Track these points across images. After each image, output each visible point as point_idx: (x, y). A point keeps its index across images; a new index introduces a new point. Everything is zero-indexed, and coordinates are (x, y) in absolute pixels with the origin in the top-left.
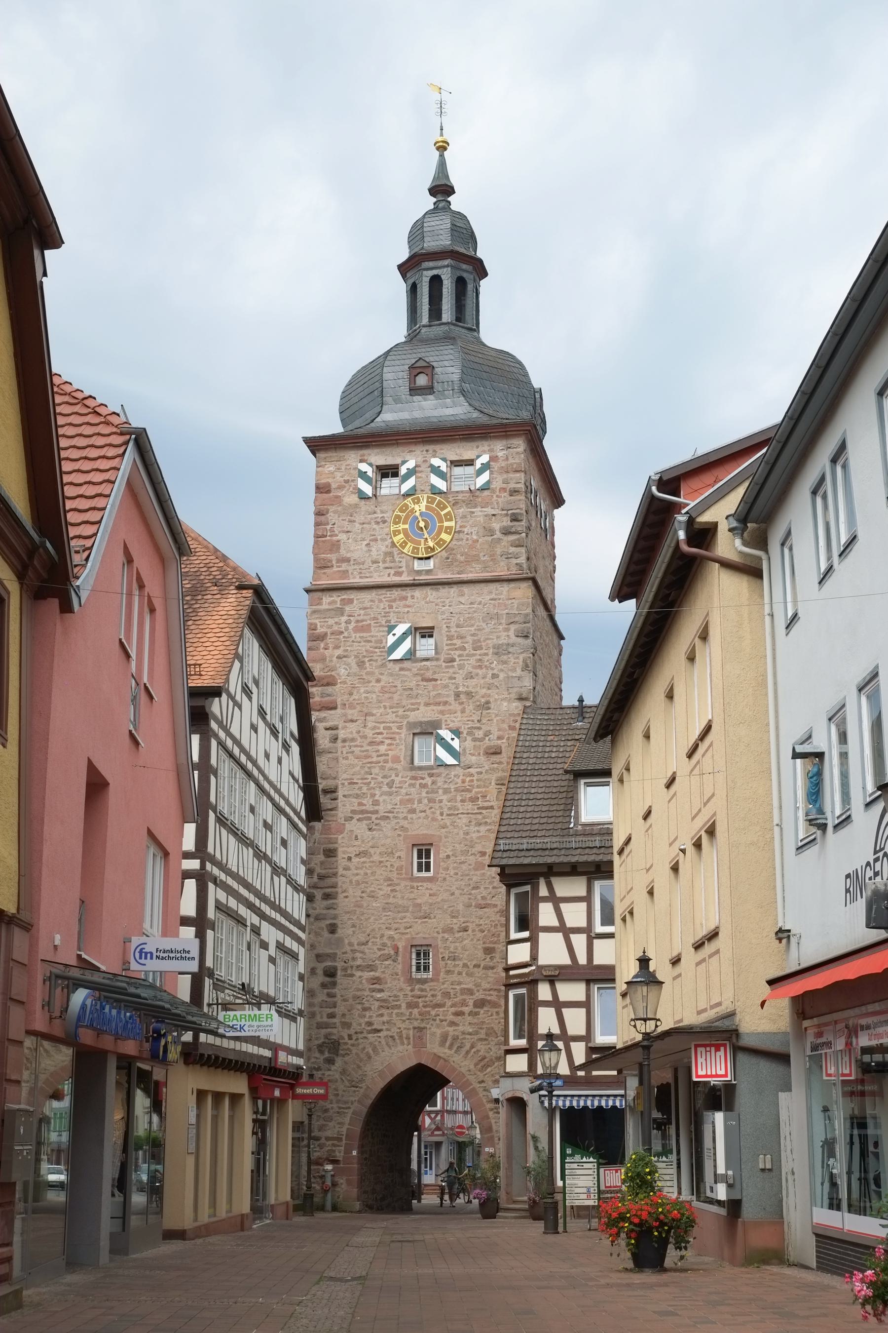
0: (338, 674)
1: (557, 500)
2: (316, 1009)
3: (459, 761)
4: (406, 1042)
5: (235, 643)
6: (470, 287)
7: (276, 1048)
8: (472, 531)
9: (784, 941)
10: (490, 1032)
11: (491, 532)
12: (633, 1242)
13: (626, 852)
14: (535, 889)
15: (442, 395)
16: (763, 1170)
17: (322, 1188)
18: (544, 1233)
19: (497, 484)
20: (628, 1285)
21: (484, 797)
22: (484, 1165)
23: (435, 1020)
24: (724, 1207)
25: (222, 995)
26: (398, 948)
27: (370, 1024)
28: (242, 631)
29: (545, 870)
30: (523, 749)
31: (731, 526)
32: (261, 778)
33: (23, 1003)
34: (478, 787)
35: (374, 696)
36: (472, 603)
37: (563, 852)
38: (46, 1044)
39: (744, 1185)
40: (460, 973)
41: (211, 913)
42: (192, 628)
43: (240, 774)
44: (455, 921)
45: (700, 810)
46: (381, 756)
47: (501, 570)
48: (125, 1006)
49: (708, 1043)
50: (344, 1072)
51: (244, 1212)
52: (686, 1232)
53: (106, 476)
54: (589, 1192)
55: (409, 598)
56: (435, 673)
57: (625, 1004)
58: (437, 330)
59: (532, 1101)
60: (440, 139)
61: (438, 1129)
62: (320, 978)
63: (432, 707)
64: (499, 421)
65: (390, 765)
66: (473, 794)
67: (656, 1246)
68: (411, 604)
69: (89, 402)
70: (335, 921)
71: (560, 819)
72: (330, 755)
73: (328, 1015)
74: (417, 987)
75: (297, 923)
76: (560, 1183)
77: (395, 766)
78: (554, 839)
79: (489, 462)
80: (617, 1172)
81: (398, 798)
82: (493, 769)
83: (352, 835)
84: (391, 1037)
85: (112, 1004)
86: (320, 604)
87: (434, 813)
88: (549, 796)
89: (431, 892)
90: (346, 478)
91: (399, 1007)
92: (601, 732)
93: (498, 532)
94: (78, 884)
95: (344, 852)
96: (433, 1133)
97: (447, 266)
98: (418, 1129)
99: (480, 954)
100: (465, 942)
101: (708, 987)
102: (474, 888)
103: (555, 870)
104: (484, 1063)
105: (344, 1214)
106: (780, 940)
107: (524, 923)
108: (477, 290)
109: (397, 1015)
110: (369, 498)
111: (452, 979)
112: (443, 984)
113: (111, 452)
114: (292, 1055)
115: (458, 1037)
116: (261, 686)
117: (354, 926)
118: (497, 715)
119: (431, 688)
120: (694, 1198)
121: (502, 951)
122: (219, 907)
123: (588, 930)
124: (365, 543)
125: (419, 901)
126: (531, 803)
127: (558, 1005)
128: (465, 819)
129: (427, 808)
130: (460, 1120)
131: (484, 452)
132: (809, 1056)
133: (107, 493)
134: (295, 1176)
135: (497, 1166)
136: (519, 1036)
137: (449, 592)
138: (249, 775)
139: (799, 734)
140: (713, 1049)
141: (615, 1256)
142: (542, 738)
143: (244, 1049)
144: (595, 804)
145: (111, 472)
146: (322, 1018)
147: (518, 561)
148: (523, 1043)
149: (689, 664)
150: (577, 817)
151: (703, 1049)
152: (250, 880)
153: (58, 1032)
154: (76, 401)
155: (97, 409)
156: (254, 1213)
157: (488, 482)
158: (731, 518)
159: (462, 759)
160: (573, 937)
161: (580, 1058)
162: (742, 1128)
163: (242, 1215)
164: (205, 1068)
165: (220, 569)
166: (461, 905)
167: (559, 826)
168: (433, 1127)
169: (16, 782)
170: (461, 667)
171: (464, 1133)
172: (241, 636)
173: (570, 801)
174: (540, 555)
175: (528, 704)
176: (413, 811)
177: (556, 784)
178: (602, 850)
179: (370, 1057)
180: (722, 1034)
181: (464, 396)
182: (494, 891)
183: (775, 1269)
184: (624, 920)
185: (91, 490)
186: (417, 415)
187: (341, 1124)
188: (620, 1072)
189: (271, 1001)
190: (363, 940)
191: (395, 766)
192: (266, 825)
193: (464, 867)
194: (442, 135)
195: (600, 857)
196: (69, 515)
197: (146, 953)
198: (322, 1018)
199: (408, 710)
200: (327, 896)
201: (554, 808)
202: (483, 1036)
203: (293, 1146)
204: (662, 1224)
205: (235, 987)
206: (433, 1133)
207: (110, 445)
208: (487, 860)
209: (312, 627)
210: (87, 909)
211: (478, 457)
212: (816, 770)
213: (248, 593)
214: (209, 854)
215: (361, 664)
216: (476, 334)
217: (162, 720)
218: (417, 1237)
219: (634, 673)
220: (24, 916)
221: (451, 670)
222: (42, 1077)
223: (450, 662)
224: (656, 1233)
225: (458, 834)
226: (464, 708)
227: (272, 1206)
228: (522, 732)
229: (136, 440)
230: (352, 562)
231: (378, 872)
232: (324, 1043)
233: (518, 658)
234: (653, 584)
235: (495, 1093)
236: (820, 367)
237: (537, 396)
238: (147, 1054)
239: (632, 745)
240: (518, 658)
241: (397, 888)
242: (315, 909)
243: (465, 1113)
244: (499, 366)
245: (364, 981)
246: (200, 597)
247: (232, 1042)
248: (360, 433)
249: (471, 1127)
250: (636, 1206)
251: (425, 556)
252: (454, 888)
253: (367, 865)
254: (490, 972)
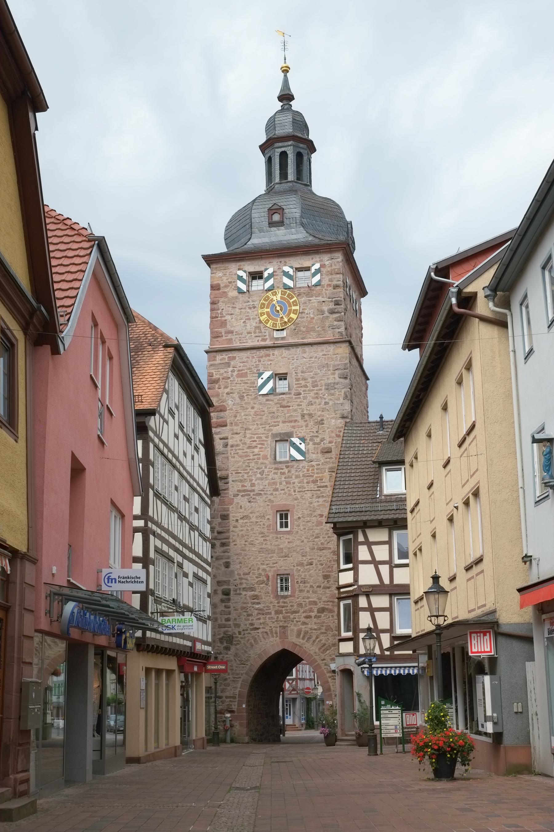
0: (227, 404)
1: (363, 292)
2: (218, 616)
3: (305, 458)
4: (275, 635)
5: (164, 381)
6: (305, 158)
7: (194, 640)
8: (310, 312)
9: (528, 563)
10: (328, 628)
11: (322, 312)
12: (434, 761)
13: (416, 511)
14: (356, 537)
15: (289, 227)
16: (516, 713)
17: (224, 729)
18: (368, 755)
19: (325, 282)
20: (434, 790)
21: (321, 480)
22: (327, 713)
23: (293, 621)
24: (490, 737)
25: (160, 607)
26: (269, 576)
27: (252, 624)
28: (168, 374)
29: (362, 525)
30: (345, 449)
31: (486, 294)
32: (181, 469)
33: (33, 611)
35: (250, 418)
36: (311, 358)
37: (373, 513)
38: (49, 639)
39: (505, 723)
40: (308, 592)
41: (152, 554)
42: (135, 372)
43: (168, 467)
44: (304, 558)
45: (468, 480)
46: (255, 455)
47: (329, 337)
48: (99, 613)
49: (479, 630)
50: (236, 655)
51: (176, 745)
52: (468, 754)
53: (79, 268)
54: (396, 728)
55: (271, 355)
56: (288, 402)
57: (417, 608)
58: (285, 186)
59: (357, 670)
60: (284, 65)
61: (294, 690)
62: (220, 596)
63: (287, 424)
64: (326, 242)
65: (261, 461)
66: (314, 478)
67: (449, 763)
68: (272, 359)
69: (68, 222)
70: (228, 560)
71: (371, 492)
72: (223, 456)
73: (225, 619)
74: (281, 600)
75: (205, 561)
76: (376, 723)
77: (265, 461)
78: (367, 505)
79: (320, 268)
80: (413, 715)
81: (267, 482)
82: (326, 462)
83: (238, 506)
84: (266, 632)
85: (91, 612)
86: (215, 360)
87: (289, 491)
88: (363, 478)
89: (289, 540)
90: (230, 280)
91: (270, 613)
92: (398, 434)
93: (326, 313)
94: (67, 533)
95: (233, 517)
96: (291, 692)
97: (291, 145)
98: (283, 690)
99: (321, 579)
100: (311, 572)
101: (476, 595)
102: (316, 538)
103: (368, 525)
104: (324, 648)
105: (238, 744)
106: (525, 562)
107: (349, 559)
108: (309, 160)
109: (269, 618)
110: (244, 292)
111: (303, 595)
112: (298, 598)
113: (82, 253)
114: (204, 645)
115: (308, 632)
116: (180, 409)
117: (240, 563)
118: (328, 428)
119: (286, 412)
120: (468, 731)
121: (335, 577)
122: (157, 550)
123: (390, 562)
124: (243, 321)
125: (281, 546)
126: (351, 483)
127: (372, 610)
128: (309, 494)
129: (285, 488)
130: (307, 684)
131: (317, 262)
132: (547, 638)
133: (80, 278)
134: (208, 721)
135: (335, 713)
136: (347, 630)
137: (296, 351)
138: (174, 466)
139: (536, 427)
140: (482, 634)
141: (422, 770)
142: (358, 442)
143: (174, 641)
144: (392, 482)
145: (82, 265)
146: (221, 621)
147: (340, 330)
148: (350, 634)
149: (457, 386)
150: (381, 491)
151: (475, 635)
152: (176, 534)
153: (56, 631)
154: (59, 221)
155: (73, 226)
156: (183, 745)
157: (320, 281)
158: (486, 289)
159: (307, 456)
160: (380, 567)
161: (386, 643)
162: (502, 686)
163: (176, 747)
164: (150, 654)
165: (153, 335)
166: (308, 548)
167: (370, 497)
168: (291, 689)
169: (25, 465)
170: (305, 398)
171: (310, 692)
172: (167, 377)
173: (376, 481)
174: (353, 327)
175: (348, 420)
176: (276, 490)
177: (367, 470)
179: (252, 646)
180: (487, 625)
181: (303, 227)
182: (328, 539)
183: (527, 777)
184: (415, 554)
185: (69, 277)
186: (274, 239)
187: (235, 688)
188: (414, 651)
189: (191, 611)
190: (246, 571)
191: (265, 461)
192: (185, 498)
193: (309, 524)
194: (285, 63)
195: (397, 516)
196: (56, 293)
197: (112, 579)
198: (221, 621)
199: (272, 426)
200: (223, 545)
201: (367, 485)
202: (323, 631)
203: (206, 702)
204: (453, 749)
205: (168, 601)
206: (291, 692)
207: (82, 248)
208: (324, 520)
209: (210, 375)
210: (73, 551)
212: (548, 450)
213: (171, 350)
214: (150, 517)
215: (242, 398)
216: (309, 188)
217: (118, 430)
218: (288, 759)
219: (420, 395)
220: (32, 554)
222: (46, 662)
223: (298, 395)
224: (449, 756)
225: (305, 503)
226: (308, 424)
227: (194, 740)
228: (345, 438)
229: (98, 244)
230: (234, 333)
231: (255, 529)
232: (223, 637)
233: (341, 391)
234: (434, 335)
235: (333, 666)
236: (549, 182)
237: (349, 226)
238: (113, 645)
239: (419, 442)
240: (341, 391)
241: (268, 538)
242: (216, 553)
243: (310, 680)
244: (325, 207)
245: (248, 598)
246: (140, 353)
247: (167, 637)
248: (238, 252)
249: (314, 688)
250: (436, 738)
251: (281, 328)
252: (303, 537)
253: (248, 524)
254: (327, 591)
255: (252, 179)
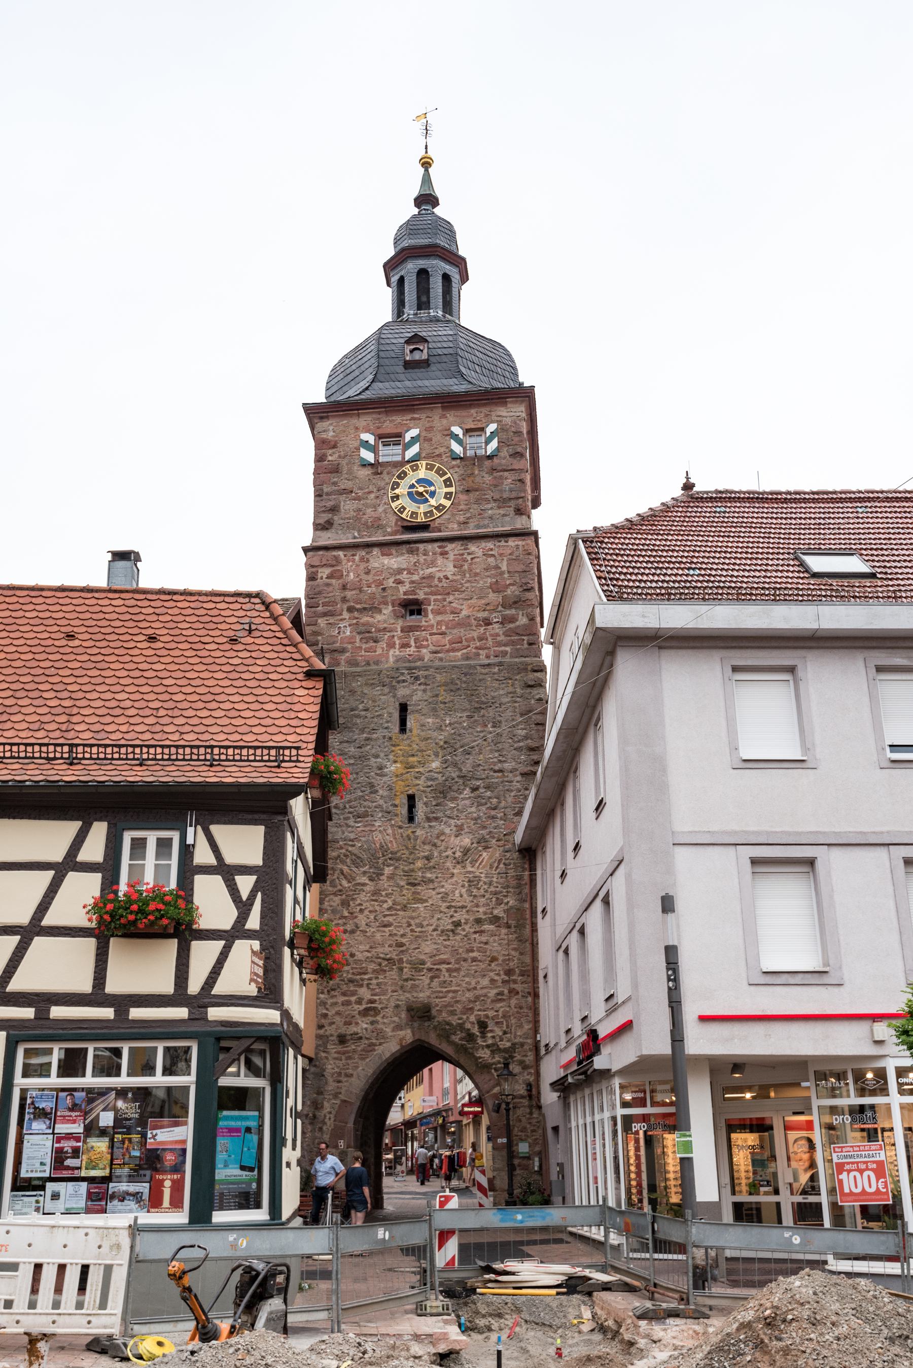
163: (493, 1148)
255: (372, 307)
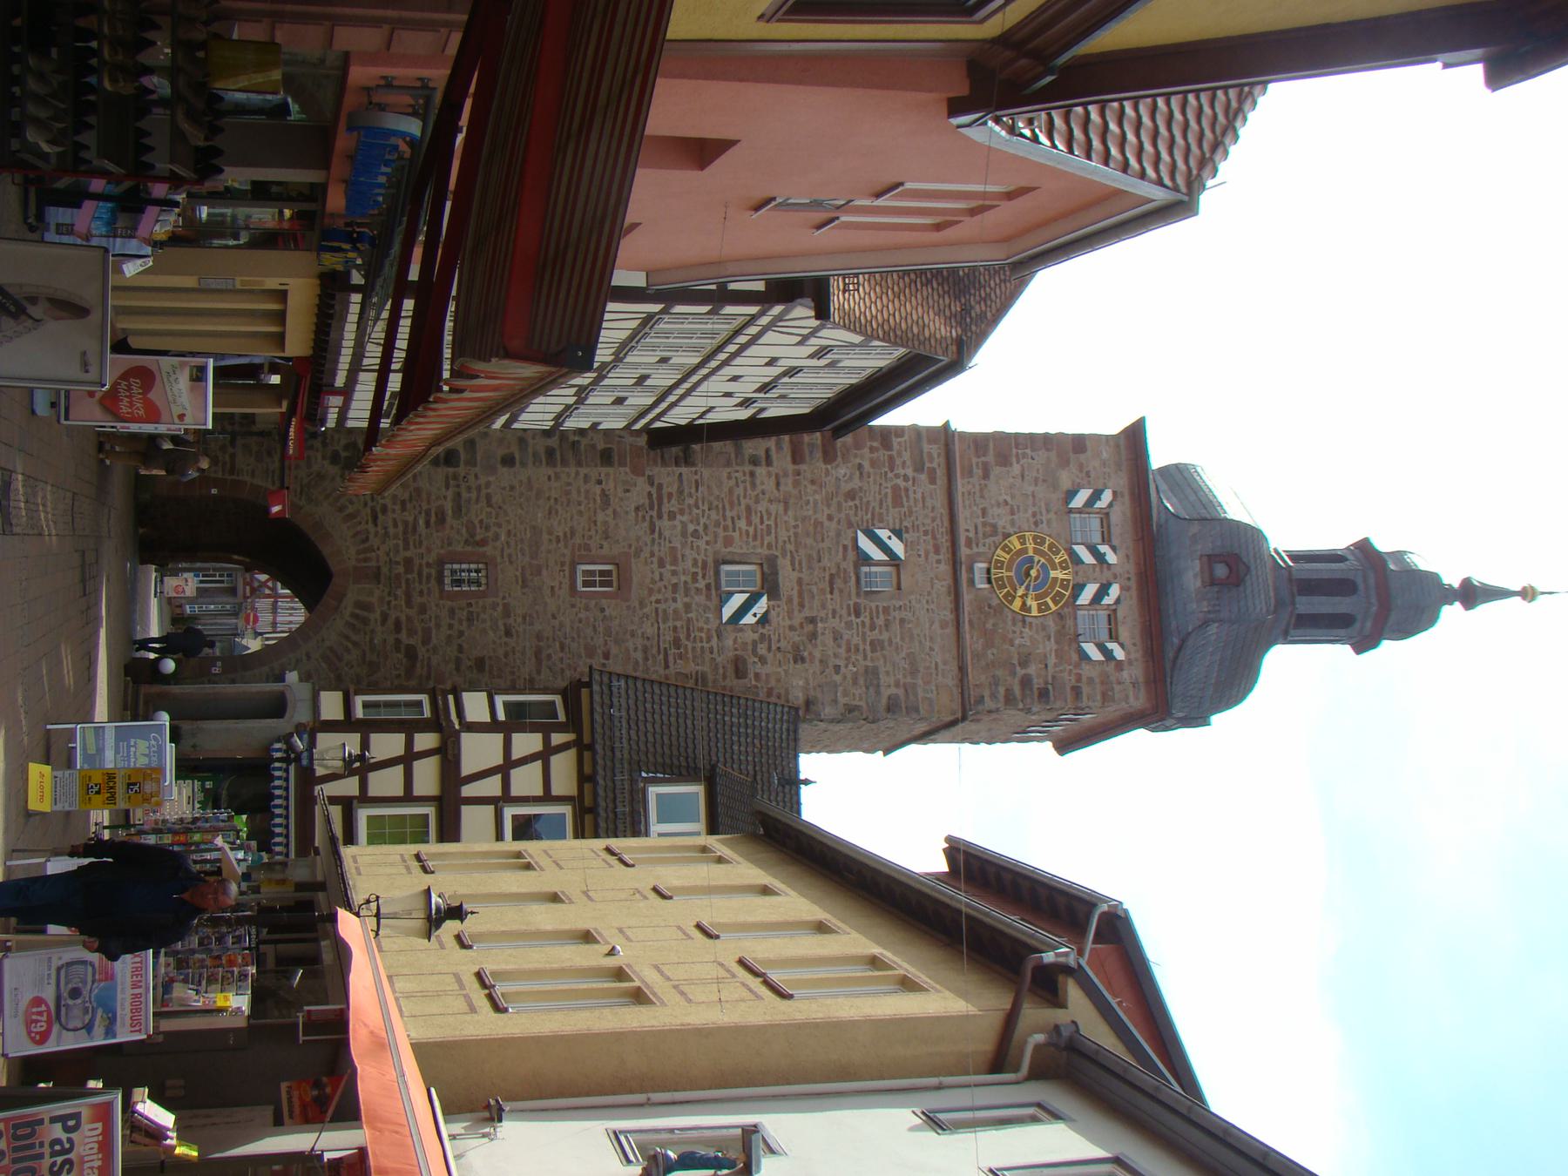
8: (1024, 638)
13: (612, 860)
14: (561, 728)
19: (1086, 671)
34: (694, 648)
40: (451, 626)
44: (520, 620)
45: (668, 979)
47: (975, 676)
56: (841, 591)
61: (253, 590)
65: (722, 534)
66: (684, 641)
77: (720, 540)
83: (629, 489)
87: (659, 591)
90: (1093, 475)
95: (607, 475)
109: (397, 545)
119: (821, 586)
123: (507, 798)
124: (1009, 499)
125: (544, 572)
126: (673, 719)
127: (408, 759)
131: (1128, 653)
143: (344, 351)
147: (987, 699)
148: (359, 713)
158: (1073, 1028)
159: (729, 628)
160: (498, 778)
168: (256, 584)
170: (849, 625)
175: (801, 713)
176: (661, 564)
178: (611, 815)
191: (720, 540)
193: (589, 631)
211: (1122, 645)
215: (851, 495)
217: (789, 243)
221: (844, 612)
241: (561, 545)
254: (452, 666)
